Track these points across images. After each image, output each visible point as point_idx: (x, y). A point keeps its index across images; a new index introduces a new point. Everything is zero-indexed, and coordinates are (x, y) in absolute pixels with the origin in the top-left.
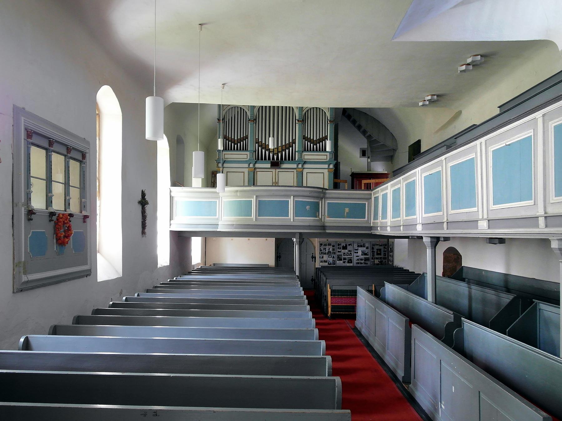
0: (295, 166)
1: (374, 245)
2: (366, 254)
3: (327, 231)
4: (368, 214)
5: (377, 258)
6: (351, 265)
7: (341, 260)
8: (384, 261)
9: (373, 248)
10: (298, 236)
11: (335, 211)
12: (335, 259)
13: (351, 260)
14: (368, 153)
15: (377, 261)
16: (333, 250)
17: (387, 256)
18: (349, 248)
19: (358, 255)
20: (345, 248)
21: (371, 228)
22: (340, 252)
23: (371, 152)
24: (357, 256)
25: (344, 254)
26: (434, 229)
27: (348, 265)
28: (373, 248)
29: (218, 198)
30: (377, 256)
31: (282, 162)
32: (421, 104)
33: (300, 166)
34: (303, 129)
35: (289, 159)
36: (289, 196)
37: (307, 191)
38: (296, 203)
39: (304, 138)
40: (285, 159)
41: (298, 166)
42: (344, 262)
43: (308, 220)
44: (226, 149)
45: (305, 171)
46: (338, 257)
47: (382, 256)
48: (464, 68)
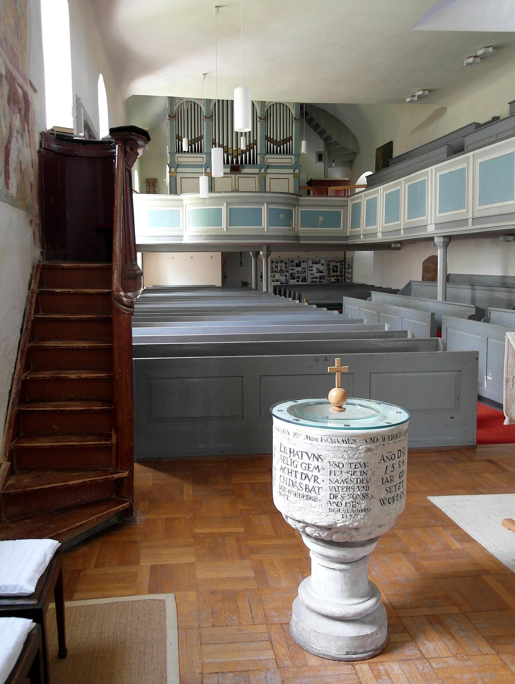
0: (256, 171)
1: (329, 261)
2: (321, 272)
3: (302, 242)
4: (343, 223)
5: (333, 276)
6: (306, 283)
7: (294, 278)
8: (341, 278)
9: (329, 265)
10: (265, 248)
11: (309, 220)
12: (287, 278)
13: (305, 278)
14: (325, 157)
15: (333, 279)
16: (286, 267)
17: (343, 274)
18: (303, 265)
19: (314, 271)
20: (298, 265)
21: (346, 238)
22: (293, 270)
23: (329, 156)
24: (312, 274)
25: (298, 272)
26: (454, 227)
27: (302, 283)
28: (329, 265)
29: (181, 206)
30: (333, 274)
31: (243, 167)
32: (408, 100)
33: (263, 171)
34: (265, 128)
35: (250, 163)
36: (262, 203)
37: (278, 197)
38: (269, 211)
39: (267, 138)
40: (246, 163)
41: (260, 171)
42: (298, 281)
43: (281, 230)
44: (179, 151)
45: (268, 177)
46: (291, 275)
47: (339, 273)
48: (471, 60)
